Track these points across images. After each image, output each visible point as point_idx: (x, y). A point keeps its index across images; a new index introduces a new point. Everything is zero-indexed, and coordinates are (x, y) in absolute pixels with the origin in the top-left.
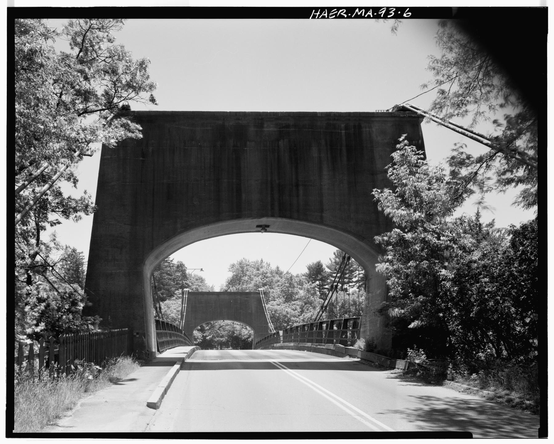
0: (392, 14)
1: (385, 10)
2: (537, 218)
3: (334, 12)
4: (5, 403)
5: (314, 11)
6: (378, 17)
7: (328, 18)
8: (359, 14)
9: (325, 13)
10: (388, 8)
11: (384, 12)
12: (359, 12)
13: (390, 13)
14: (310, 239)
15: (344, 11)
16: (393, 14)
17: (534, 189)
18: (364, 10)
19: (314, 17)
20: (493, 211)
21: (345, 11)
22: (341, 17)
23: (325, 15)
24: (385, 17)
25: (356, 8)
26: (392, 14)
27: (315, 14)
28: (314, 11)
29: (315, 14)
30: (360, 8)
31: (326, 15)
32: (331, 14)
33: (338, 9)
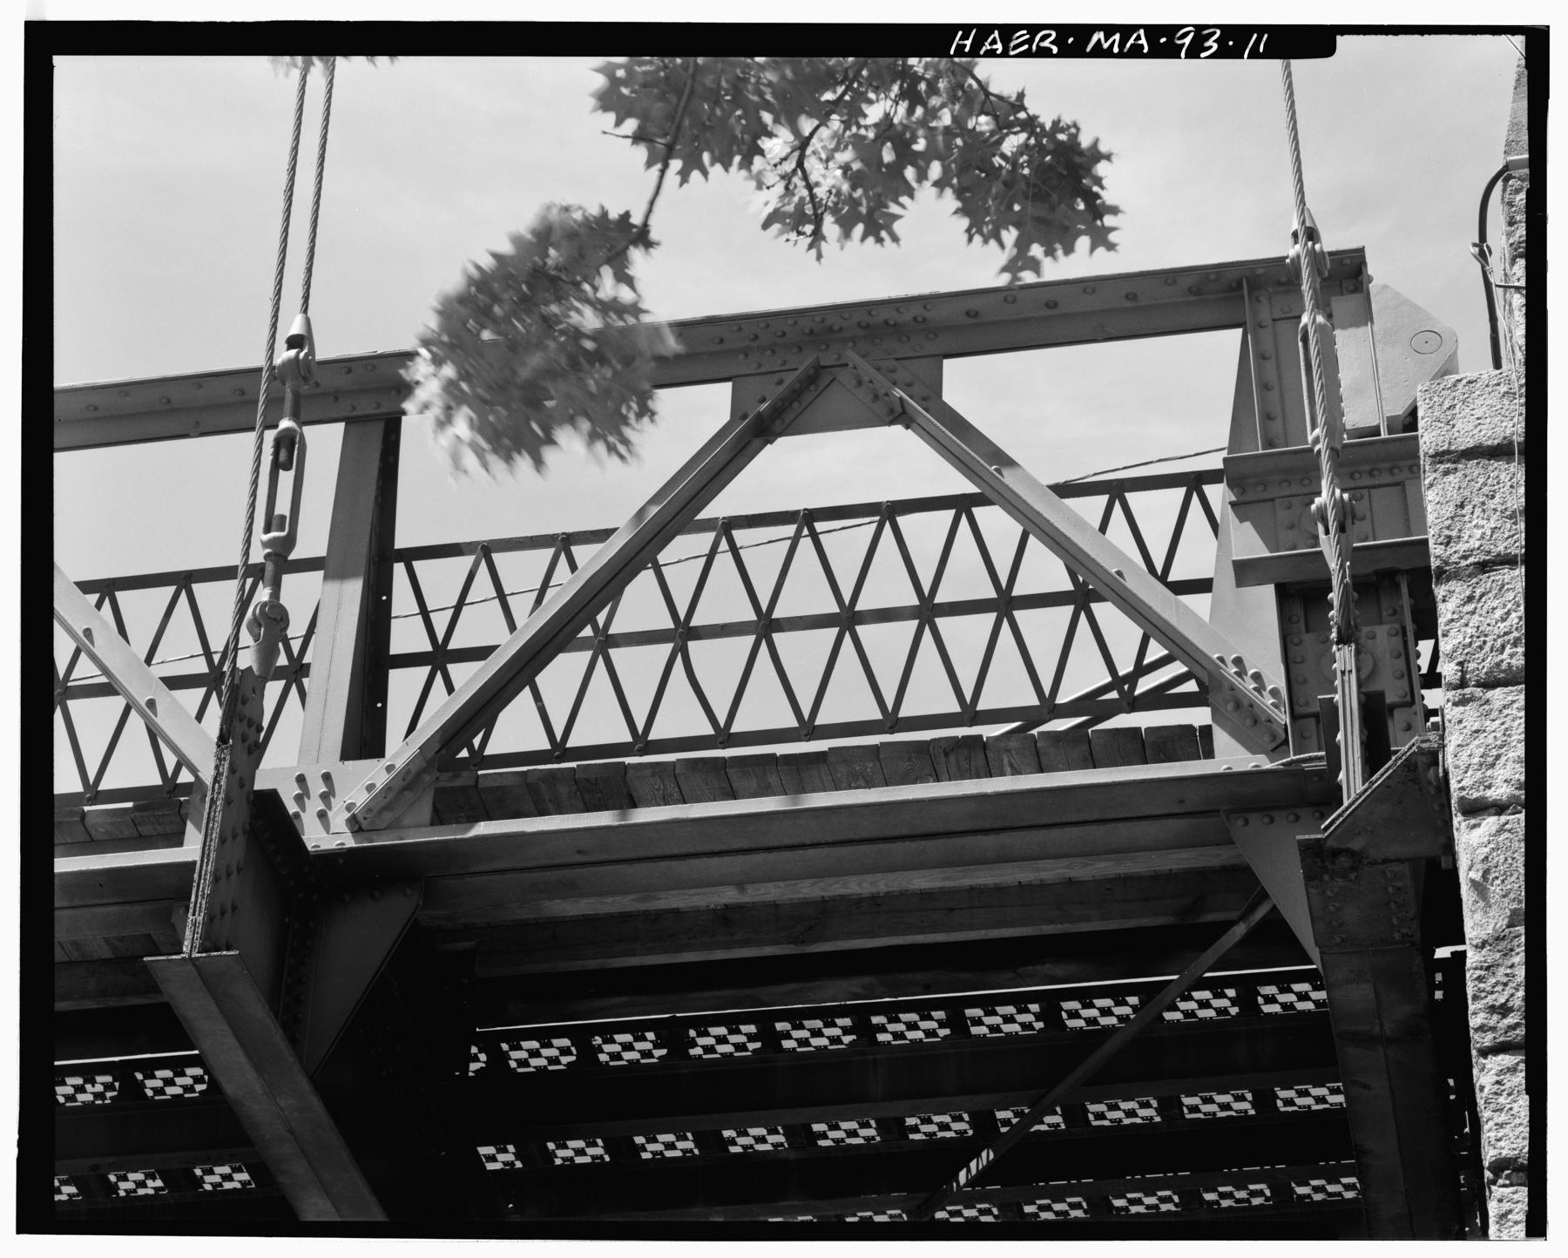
0: (1211, 47)
1: (1192, 35)
2: (562, 648)
3: (1023, 35)
4: (17, 1137)
5: (960, 33)
6: (1171, 52)
7: (1005, 54)
8: (1106, 46)
9: (994, 42)
10: (1199, 28)
11: (1187, 40)
12: (1106, 41)
13: (1207, 44)
14: (237, 1045)
15: (1050, 35)
16: (1215, 46)
17: (1397, 626)
18: (1117, 37)
19: (1254, 54)
20: (296, 629)
21: (1218, 32)
22: (1044, 53)
23: (995, 47)
24: (1194, 52)
25: (956, 27)
26: (1211, 47)
27: (961, 42)
28: (960, 33)
29: (961, 42)
30: (1109, 30)
31: (999, 47)
32: (1012, 44)
33: (1033, 29)
